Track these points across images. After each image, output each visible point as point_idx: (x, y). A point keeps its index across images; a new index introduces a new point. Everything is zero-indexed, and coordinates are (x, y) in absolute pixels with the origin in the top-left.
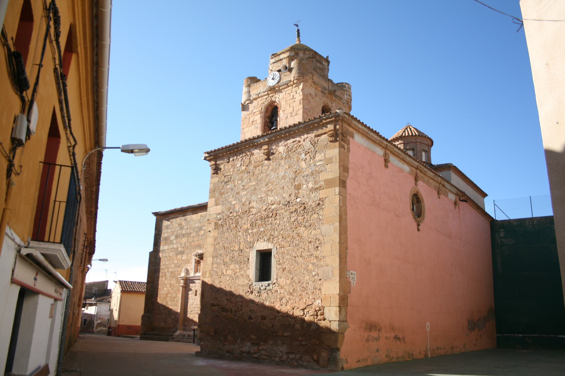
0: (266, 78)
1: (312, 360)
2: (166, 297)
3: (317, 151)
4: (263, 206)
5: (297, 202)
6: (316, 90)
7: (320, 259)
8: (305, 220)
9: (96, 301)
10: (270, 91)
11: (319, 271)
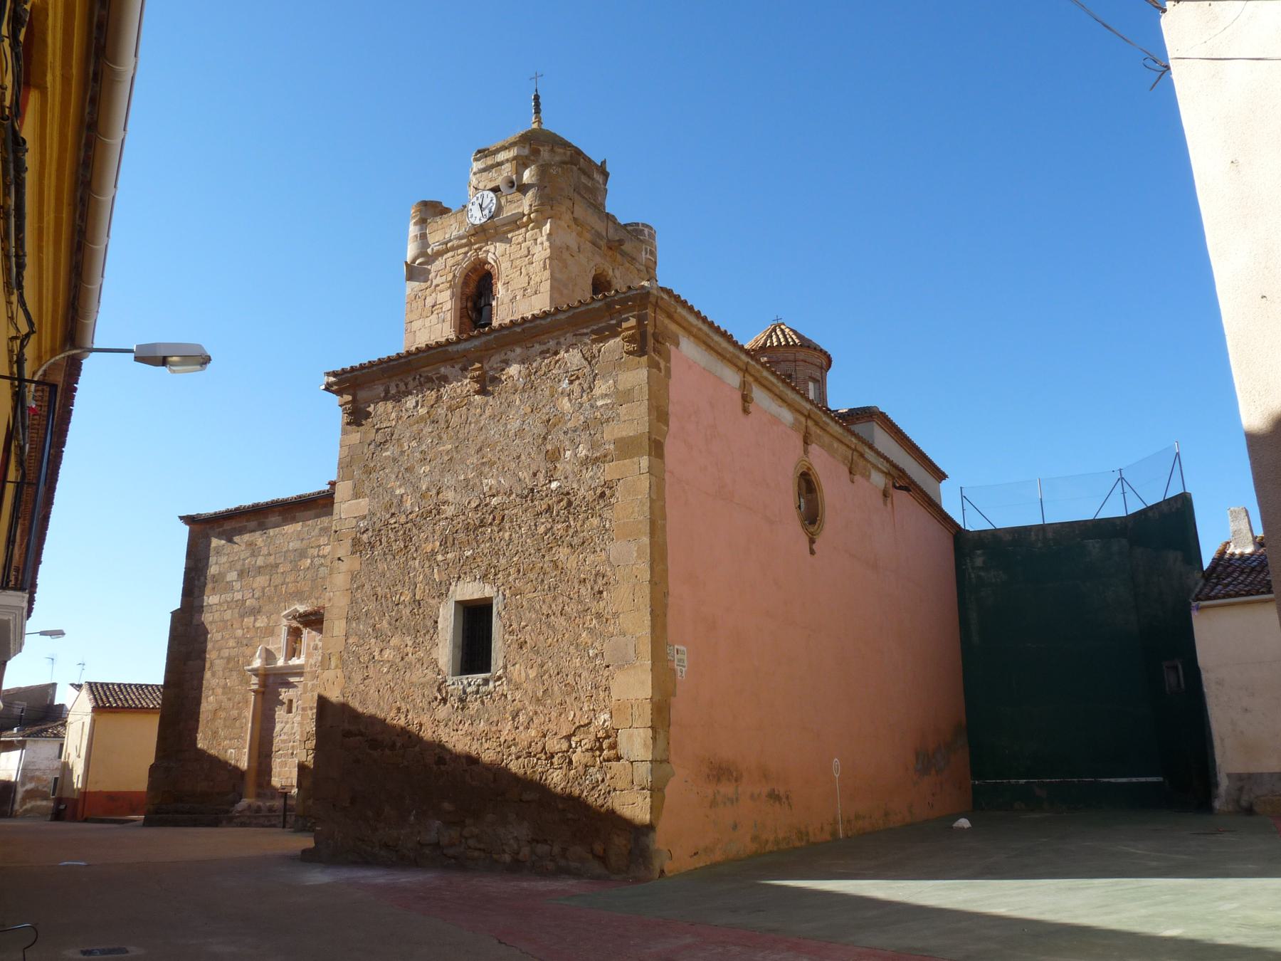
0: (465, 207)
1: (590, 856)
2: (213, 720)
3: (596, 374)
4: (471, 500)
5: (552, 491)
6: (580, 237)
7: (607, 620)
8: (571, 532)
9: (23, 736)
10: (473, 235)
11: (604, 645)
